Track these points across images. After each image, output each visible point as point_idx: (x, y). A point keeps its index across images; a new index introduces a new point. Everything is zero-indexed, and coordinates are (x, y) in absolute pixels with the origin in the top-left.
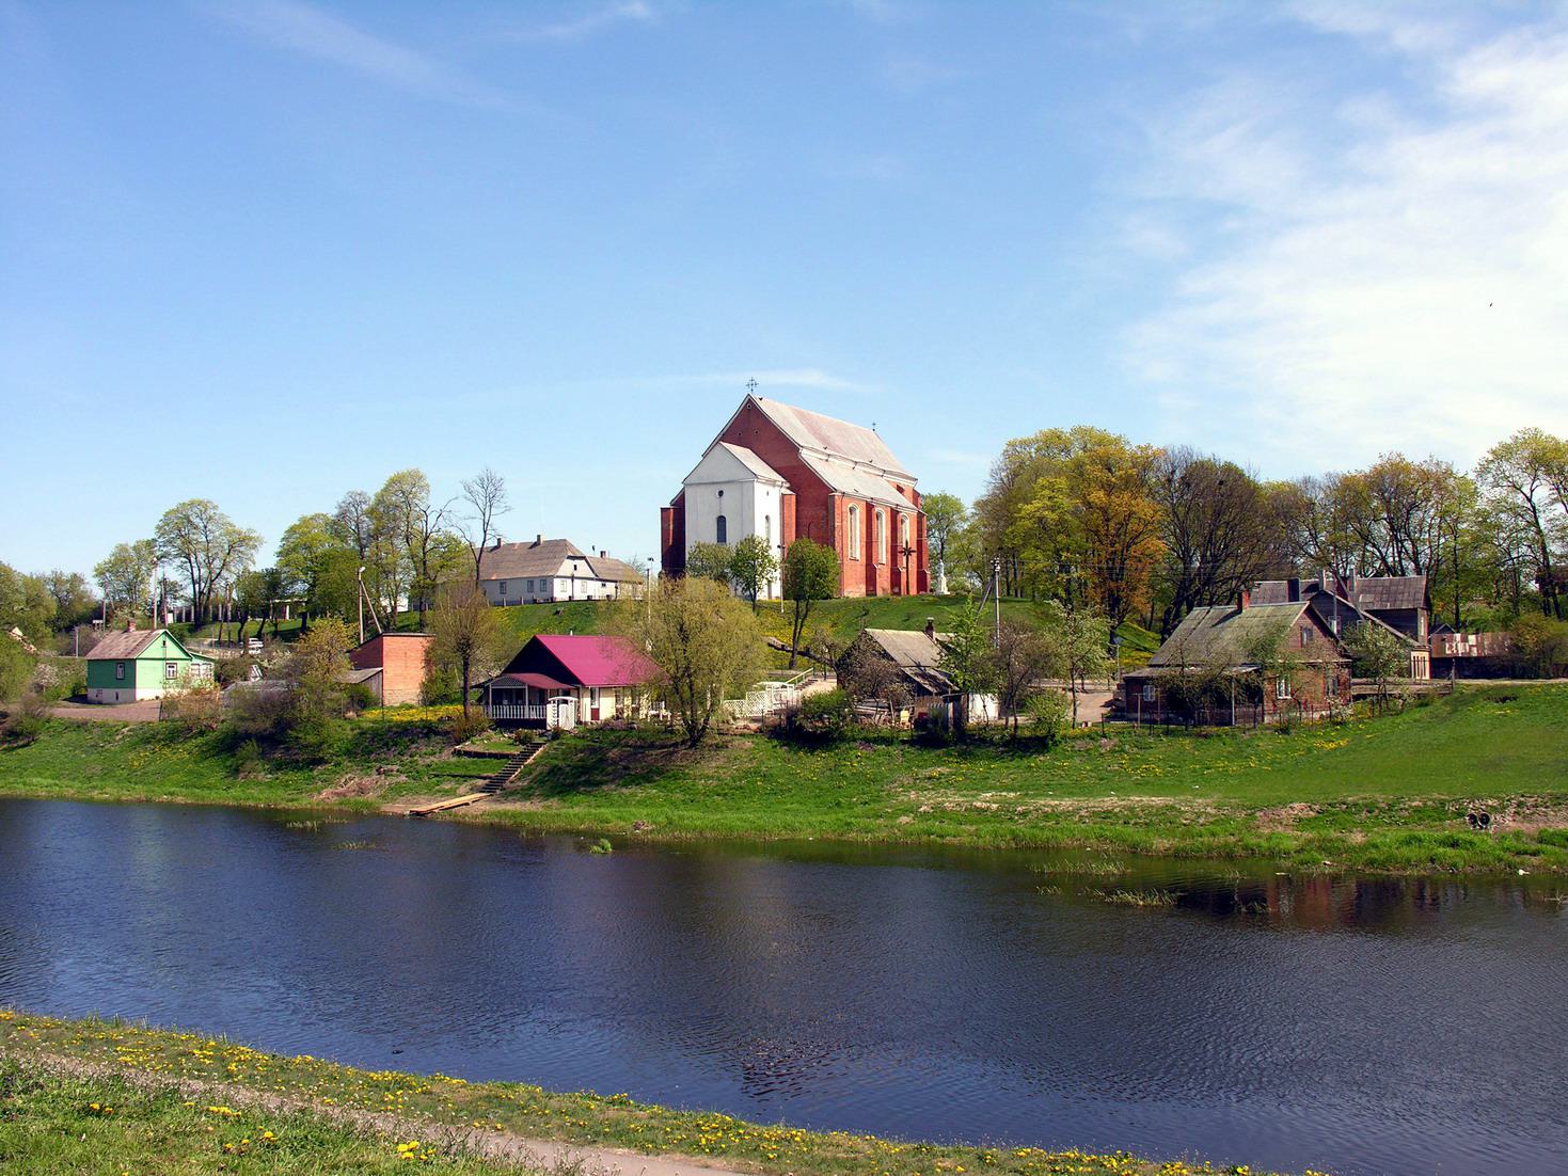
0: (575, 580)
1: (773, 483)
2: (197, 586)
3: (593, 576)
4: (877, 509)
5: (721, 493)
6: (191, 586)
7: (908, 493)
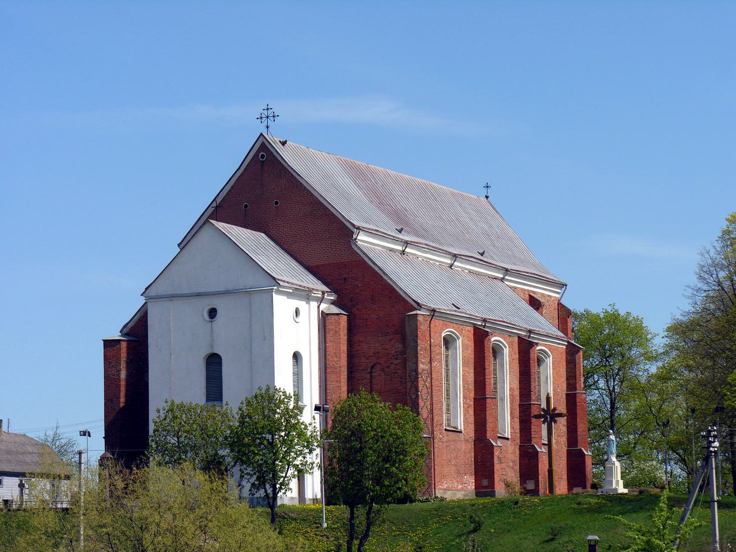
5: (213, 313)
7: (551, 310)
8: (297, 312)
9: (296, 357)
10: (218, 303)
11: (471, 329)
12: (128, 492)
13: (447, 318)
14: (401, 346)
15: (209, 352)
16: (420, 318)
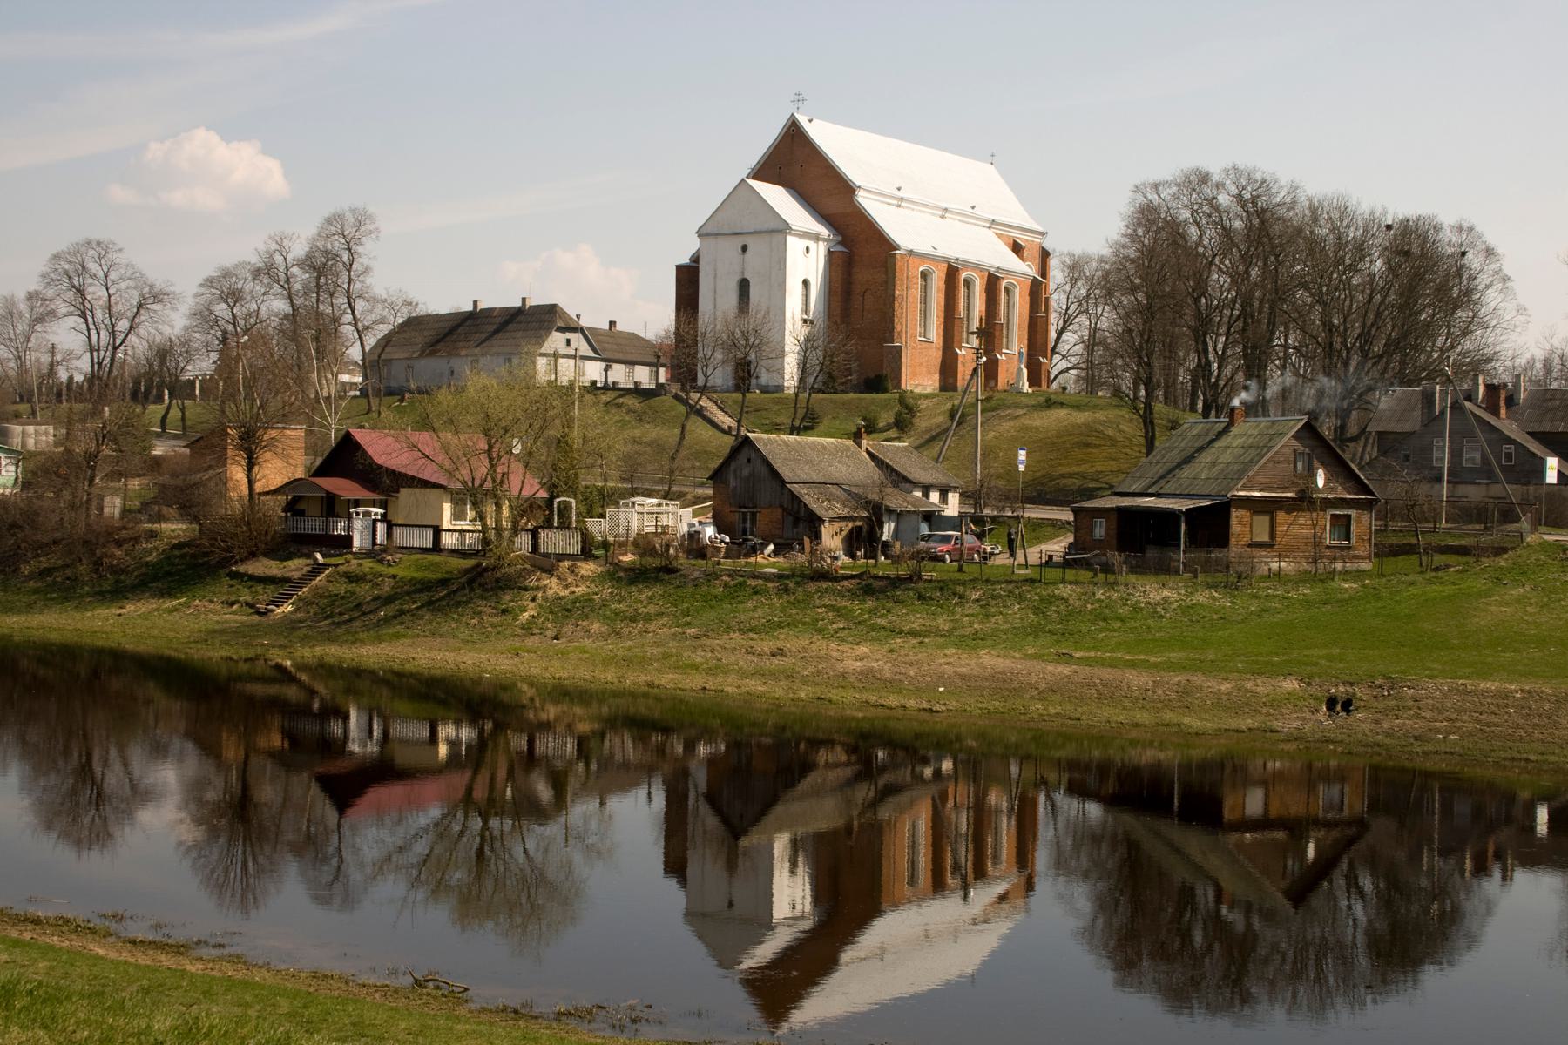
0: (561, 361)
1: (816, 238)
2: (95, 354)
3: (592, 354)
4: (963, 275)
5: (744, 248)
6: (88, 354)
7: (1031, 252)
8: (808, 249)
9: (806, 283)
10: (748, 240)
11: (946, 265)
12: (667, 664)
13: (923, 256)
14: (884, 276)
15: (741, 277)
16: (898, 257)
